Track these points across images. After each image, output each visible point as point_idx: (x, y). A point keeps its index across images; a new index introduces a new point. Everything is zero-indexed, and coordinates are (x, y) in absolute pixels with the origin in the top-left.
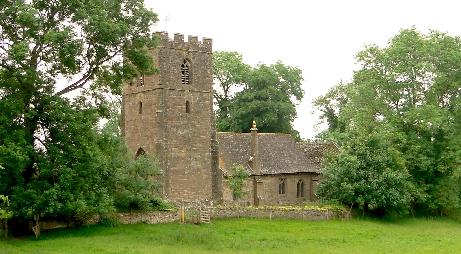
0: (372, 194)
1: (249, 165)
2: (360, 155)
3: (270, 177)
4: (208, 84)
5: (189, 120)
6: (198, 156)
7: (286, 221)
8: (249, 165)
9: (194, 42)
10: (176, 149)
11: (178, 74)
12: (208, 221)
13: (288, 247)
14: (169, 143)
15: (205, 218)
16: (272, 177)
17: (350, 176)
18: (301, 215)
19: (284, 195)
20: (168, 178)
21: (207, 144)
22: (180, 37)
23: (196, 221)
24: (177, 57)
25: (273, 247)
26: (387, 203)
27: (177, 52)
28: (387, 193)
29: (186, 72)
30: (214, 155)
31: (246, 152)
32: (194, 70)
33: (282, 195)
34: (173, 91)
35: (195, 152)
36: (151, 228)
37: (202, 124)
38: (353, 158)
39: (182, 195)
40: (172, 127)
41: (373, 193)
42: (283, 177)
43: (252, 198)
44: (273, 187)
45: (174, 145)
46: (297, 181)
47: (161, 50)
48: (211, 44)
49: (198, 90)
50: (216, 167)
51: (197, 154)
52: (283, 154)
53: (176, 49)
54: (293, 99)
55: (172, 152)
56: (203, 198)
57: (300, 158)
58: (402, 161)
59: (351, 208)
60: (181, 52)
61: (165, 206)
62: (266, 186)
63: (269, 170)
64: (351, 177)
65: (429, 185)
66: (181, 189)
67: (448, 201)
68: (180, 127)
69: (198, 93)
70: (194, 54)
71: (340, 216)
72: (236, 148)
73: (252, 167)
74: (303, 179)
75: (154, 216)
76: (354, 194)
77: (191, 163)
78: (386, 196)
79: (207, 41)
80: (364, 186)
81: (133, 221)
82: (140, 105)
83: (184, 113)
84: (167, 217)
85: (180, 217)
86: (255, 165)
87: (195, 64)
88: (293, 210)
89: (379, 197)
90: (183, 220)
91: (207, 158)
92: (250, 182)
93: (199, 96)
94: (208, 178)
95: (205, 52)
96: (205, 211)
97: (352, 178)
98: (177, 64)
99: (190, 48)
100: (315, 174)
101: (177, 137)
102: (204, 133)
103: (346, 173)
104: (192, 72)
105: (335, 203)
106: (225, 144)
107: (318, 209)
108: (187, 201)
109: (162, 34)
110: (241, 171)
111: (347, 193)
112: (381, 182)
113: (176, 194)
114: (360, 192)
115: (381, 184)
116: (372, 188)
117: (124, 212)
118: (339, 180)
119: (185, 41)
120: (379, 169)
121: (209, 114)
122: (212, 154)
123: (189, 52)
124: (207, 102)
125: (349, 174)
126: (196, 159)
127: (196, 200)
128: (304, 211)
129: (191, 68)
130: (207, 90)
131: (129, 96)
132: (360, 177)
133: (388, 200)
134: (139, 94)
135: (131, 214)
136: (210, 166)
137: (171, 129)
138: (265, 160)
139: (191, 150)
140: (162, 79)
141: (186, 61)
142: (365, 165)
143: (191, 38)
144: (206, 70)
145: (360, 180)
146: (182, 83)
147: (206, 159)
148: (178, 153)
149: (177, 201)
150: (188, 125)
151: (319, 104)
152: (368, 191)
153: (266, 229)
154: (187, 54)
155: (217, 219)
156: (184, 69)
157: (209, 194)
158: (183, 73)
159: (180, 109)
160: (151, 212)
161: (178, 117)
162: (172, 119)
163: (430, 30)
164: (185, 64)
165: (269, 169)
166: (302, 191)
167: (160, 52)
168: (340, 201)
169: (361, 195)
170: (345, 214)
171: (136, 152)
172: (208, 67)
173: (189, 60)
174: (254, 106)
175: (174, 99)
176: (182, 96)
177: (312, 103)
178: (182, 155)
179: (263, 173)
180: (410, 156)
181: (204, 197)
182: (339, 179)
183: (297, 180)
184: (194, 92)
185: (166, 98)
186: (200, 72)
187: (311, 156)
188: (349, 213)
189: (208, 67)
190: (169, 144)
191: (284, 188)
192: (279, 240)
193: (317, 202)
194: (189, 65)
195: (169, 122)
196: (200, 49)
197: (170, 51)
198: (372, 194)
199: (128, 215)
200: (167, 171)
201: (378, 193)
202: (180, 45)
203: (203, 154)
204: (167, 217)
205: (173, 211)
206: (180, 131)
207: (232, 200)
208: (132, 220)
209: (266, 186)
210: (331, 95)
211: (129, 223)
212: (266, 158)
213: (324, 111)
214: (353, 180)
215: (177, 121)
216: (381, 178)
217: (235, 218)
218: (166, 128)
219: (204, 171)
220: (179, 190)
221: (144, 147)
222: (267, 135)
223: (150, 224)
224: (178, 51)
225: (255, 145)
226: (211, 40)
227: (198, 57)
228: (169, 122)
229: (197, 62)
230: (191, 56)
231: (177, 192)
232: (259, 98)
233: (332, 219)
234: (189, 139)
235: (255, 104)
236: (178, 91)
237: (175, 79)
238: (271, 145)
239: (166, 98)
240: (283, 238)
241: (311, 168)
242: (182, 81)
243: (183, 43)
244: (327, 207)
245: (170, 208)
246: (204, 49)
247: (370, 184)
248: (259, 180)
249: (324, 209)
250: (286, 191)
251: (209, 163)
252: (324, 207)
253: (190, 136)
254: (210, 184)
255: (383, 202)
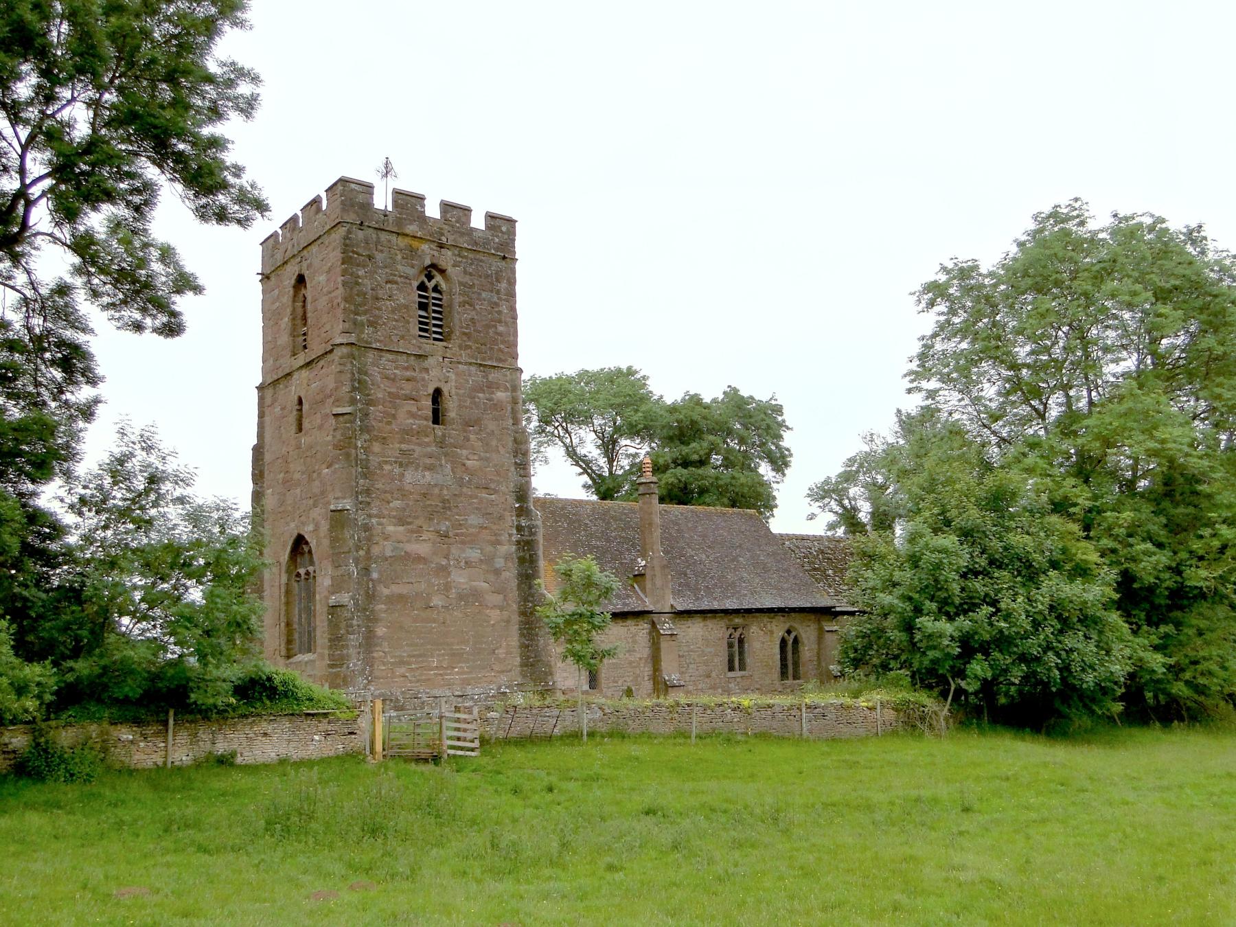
0: (1015, 649)
1: (636, 586)
2: (966, 534)
3: (700, 620)
4: (502, 343)
5: (441, 443)
6: (474, 554)
7: (746, 742)
8: (636, 586)
9: (457, 222)
10: (401, 528)
11: (406, 307)
12: (472, 750)
13: (738, 845)
14: (374, 511)
15: (465, 740)
16: (705, 619)
17: (943, 595)
18: (796, 724)
19: (742, 672)
20: (371, 619)
21: (501, 518)
22: (413, 200)
23: (425, 752)
24: (403, 258)
25: (675, 847)
26: (1063, 679)
27: (402, 242)
28: (1060, 646)
29: (434, 305)
30: (524, 551)
31: (628, 550)
32: (458, 299)
33: (737, 673)
34: (390, 357)
35: (463, 543)
36: (242, 781)
37: (487, 459)
38: (949, 541)
39: (421, 675)
40: (386, 462)
41: (1017, 646)
42: (738, 620)
43: (647, 683)
44: (709, 650)
45: (394, 517)
46: (779, 633)
47: (349, 232)
48: (511, 234)
49: (472, 357)
50: (530, 587)
51: (472, 548)
52: (734, 559)
53: (398, 234)
54: (765, 469)
55: (386, 539)
56: (491, 682)
57: (785, 570)
58: (1088, 553)
59: (950, 698)
60: (415, 243)
61: (311, 700)
62: (689, 646)
63: (698, 599)
64: (945, 598)
65: (1163, 629)
66: (414, 656)
67: (1222, 674)
68: (413, 463)
69: (473, 369)
70: (459, 255)
71: (918, 724)
72: (599, 539)
73: (645, 588)
74: (796, 625)
75: (265, 734)
76: (959, 650)
77: (449, 573)
78: (1058, 655)
79: (498, 222)
80: (988, 628)
81: (177, 755)
82: (298, 407)
83: (425, 423)
84: (316, 738)
85: (367, 736)
86: (654, 584)
87: (461, 284)
88: (770, 706)
89: (1037, 659)
90: (379, 747)
91: (502, 560)
92: (641, 634)
93: (476, 376)
94: (508, 621)
95: (493, 252)
96: (465, 713)
97: (945, 602)
98: (401, 276)
99: (443, 234)
100: (828, 613)
101: (404, 494)
102: (492, 486)
103: (927, 587)
104: (450, 306)
105: (901, 683)
106: (564, 528)
107: (848, 701)
108: (436, 692)
109: (353, 186)
110: (589, 577)
111: (935, 648)
112: (1040, 612)
113: (401, 670)
114: (977, 646)
115: (1039, 618)
116: (1014, 629)
117: (137, 722)
118: (908, 609)
119: (428, 214)
120: (1030, 573)
121: (508, 429)
122: (519, 549)
123: (441, 246)
124: (501, 395)
125: (940, 589)
126: (466, 563)
127: (469, 690)
128: (804, 710)
129: (450, 293)
130: (500, 360)
131: (275, 389)
132: (971, 598)
133: (1065, 669)
134: (296, 376)
135: (167, 731)
136: (514, 583)
137: (382, 469)
138: (686, 575)
139: (451, 534)
140: (352, 316)
141: (434, 272)
142: (983, 562)
143: (446, 207)
144: (497, 304)
145: (973, 607)
146: (420, 336)
147: (499, 563)
148: (408, 541)
149: (403, 693)
150: (440, 460)
151: (823, 498)
152: (1002, 642)
153: (674, 769)
154: (436, 254)
155: (507, 742)
156: (426, 298)
157: (510, 671)
158: (423, 306)
159: (414, 409)
160: (250, 720)
161: (406, 432)
162: (384, 438)
163: (1115, 216)
164: (429, 281)
165: (695, 596)
166: (796, 664)
167: (346, 238)
168: (913, 677)
169: (979, 656)
170: (933, 716)
171: (289, 549)
172: (504, 297)
173: (442, 272)
174: (671, 480)
175: (393, 380)
176: (421, 372)
177: (809, 496)
178: (422, 549)
179: (680, 608)
180: (1107, 543)
181: (494, 679)
182: (908, 607)
183: (778, 628)
184: (459, 363)
185: (366, 374)
186: (477, 307)
187: (815, 569)
188: (946, 712)
189: (504, 297)
190: (375, 512)
191: (741, 653)
192: (713, 810)
193: (843, 683)
194: (443, 286)
195: (376, 447)
196: (476, 243)
197: (378, 238)
198: (1015, 649)
199: (156, 734)
200: (371, 597)
201: (1033, 646)
202: (411, 224)
203: (489, 549)
204: (316, 738)
205: (340, 715)
206: (410, 476)
207: (586, 687)
208: (170, 752)
209: (689, 646)
210: (848, 477)
211: (160, 764)
212: (688, 567)
213: (836, 513)
214: (952, 610)
215: (403, 446)
216: (1041, 598)
217: (574, 737)
218: (365, 464)
219: (497, 599)
220: (409, 656)
221: (307, 532)
222: (692, 511)
223: (246, 766)
224: (407, 240)
225: (650, 524)
226: (511, 222)
227: (471, 264)
228: (376, 447)
229: (467, 279)
230: (447, 259)
231: (402, 663)
232: (686, 464)
233: (894, 733)
234: (443, 501)
235: (675, 475)
236: (405, 357)
237: (396, 321)
238: (704, 536)
239: (366, 374)
240: (726, 801)
241: (818, 596)
242: (421, 330)
243: (423, 219)
244: (878, 696)
245: (332, 705)
246: (489, 244)
247: (1007, 617)
248: (666, 627)
249: (868, 701)
250: (749, 660)
251: (510, 575)
252: (868, 697)
253: (445, 492)
254: (514, 640)
255: (1052, 675)
